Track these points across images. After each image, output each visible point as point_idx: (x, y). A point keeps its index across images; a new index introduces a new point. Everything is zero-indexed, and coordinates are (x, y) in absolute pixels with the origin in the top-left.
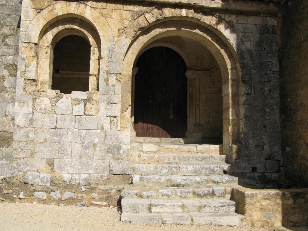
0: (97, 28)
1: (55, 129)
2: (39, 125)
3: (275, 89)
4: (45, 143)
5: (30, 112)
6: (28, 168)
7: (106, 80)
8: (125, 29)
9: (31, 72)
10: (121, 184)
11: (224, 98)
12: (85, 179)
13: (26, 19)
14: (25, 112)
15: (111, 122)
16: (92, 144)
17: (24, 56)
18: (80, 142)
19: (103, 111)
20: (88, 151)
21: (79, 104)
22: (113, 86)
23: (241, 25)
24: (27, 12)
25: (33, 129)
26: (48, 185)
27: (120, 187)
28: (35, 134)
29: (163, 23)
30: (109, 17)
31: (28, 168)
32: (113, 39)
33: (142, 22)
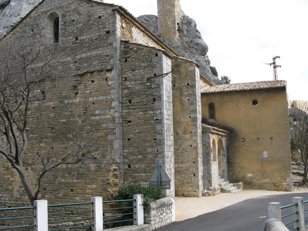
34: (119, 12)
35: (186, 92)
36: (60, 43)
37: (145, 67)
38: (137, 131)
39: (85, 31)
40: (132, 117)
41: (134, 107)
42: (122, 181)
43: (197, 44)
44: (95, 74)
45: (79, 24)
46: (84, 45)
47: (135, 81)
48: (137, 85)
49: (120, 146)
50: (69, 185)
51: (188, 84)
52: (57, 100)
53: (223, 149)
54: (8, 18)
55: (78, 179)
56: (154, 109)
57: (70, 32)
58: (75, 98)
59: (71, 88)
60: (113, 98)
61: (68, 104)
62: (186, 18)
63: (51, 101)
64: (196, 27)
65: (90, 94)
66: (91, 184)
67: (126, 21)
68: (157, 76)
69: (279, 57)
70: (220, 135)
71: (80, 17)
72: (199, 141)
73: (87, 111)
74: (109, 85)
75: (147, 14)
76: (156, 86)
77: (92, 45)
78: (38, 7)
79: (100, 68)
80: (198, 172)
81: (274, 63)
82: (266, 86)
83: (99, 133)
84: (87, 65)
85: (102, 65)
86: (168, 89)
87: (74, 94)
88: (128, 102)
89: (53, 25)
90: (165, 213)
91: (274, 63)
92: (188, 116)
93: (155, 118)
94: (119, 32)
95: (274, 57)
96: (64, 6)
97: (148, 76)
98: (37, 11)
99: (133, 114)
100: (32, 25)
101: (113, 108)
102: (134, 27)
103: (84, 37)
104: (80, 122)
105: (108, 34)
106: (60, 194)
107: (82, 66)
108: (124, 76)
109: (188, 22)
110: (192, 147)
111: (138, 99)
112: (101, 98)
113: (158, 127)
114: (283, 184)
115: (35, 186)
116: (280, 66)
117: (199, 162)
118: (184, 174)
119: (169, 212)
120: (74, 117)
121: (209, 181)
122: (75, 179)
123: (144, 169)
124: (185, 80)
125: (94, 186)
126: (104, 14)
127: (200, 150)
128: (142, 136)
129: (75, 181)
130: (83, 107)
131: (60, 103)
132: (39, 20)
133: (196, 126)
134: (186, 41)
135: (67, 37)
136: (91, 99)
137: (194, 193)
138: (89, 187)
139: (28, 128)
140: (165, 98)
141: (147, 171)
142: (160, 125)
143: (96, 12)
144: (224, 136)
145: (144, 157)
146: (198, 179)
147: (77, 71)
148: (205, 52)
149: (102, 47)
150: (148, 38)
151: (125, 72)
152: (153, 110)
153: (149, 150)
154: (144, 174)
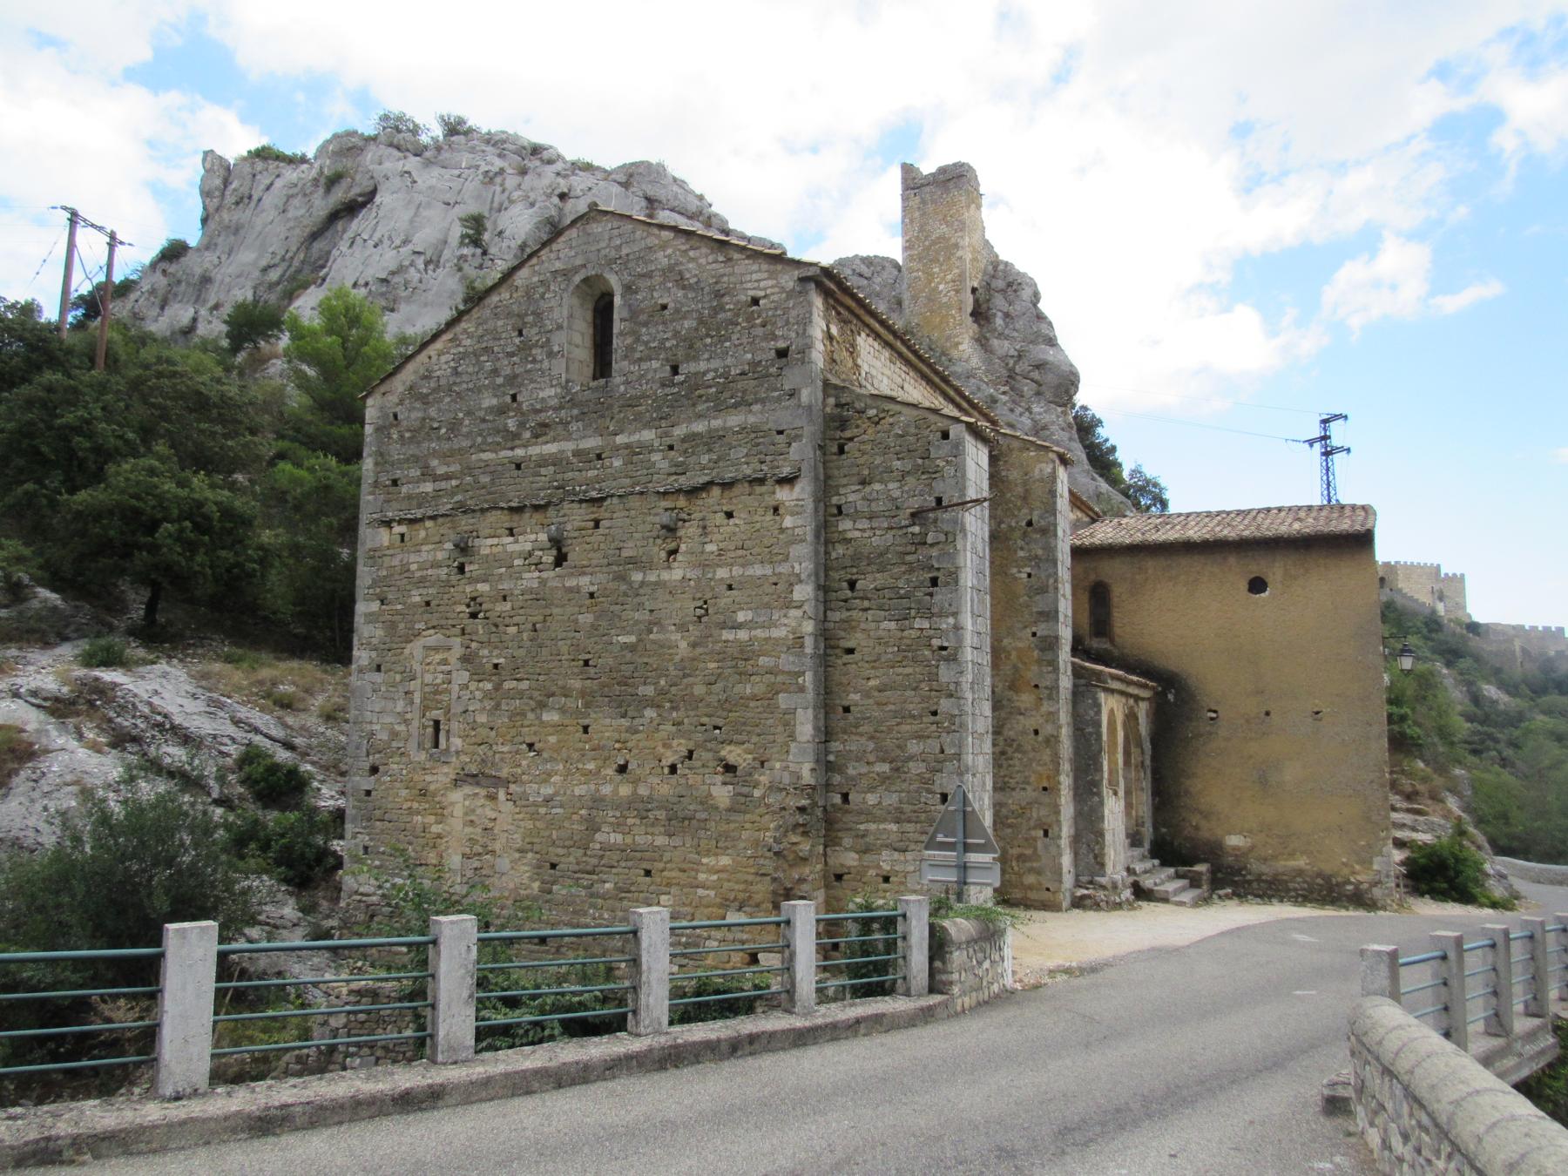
34: (820, 286)
35: (1022, 549)
36: (617, 379)
37: (904, 475)
38: (872, 683)
39: (706, 345)
40: (858, 635)
41: (866, 604)
42: (821, 847)
43: (1040, 366)
44: (737, 490)
45: (684, 318)
46: (701, 392)
47: (870, 518)
48: (878, 532)
49: (816, 728)
50: (638, 855)
51: (1030, 524)
52: (605, 569)
53: (1140, 745)
54: (368, 253)
55: (670, 836)
56: (933, 615)
57: (653, 345)
58: (669, 568)
59: (654, 534)
60: (797, 570)
61: (642, 584)
62: (1004, 271)
63: (584, 574)
64: (1038, 301)
65: (720, 555)
66: (716, 855)
67: (838, 313)
68: (946, 507)
69: (1346, 417)
70: (1131, 696)
71: (685, 296)
72: (1064, 717)
73: (707, 610)
74: (782, 530)
75: (864, 254)
76: (942, 538)
77: (728, 394)
78: (542, 253)
79: (755, 471)
80: (1059, 822)
81: (1325, 438)
82: (1297, 526)
83: (748, 686)
84: (710, 460)
85: (762, 463)
86: (980, 548)
87: (663, 555)
88: (845, 585)
89: (589, 316)
90: (988, 961)
91: (1325, 438)
92: (1029, 631)
93: (936, 642)
94: (818, 356)
95: (1326, 417)
96: (631, 257)
97: (915, 503)
98: (537, 268)
99: (863, 626)
100: (518, 316)
101: (794, 604)
102: (863, 335)
103: (703, 366)
104: (683, 645)
105: (784, 360)
106: (607, 885)
107: (692, 460)
108: (835, 500)
109: (1010, 285)
110: (1040, 738)
111: (881, 579)
112: (758, 570)
113: (945, 674)
114: (1359, 878)
115: (517, 855)
116: (1348, 450)
117: (1062, 787)
118: (1010, 826)
119: (997, 958)
120: (662, 629)
121: (1096, 857)
122: (660, 834)
123: (896, 809)
124: (1020, 510)
125: (725, 861)
126: (768, 292)
127: (1066, 747)
128: (892, 700)
129: (661, 841)
130: (694, 599)
131: (613, 580)
132: (542, 297)
133: (1053, 664)
134: (1000, 352)
135: (640, 359)
136: (722, 573)
137: (1046, 896)
138: (707, 864)
139: (502, 660)
140: (968, 579)
141: (903, 817)
142: (953, 665)
143: (742, 283)
144: (1143, 699)
145: (897, 770)
146: (1059, 846)
147: (675, 477)
148: (1067, 392)
149: (763, 401)
150: (904, 368)
151: (837, 487)
152: (931, 616)
153: (914, 747)
154: (894, 827)
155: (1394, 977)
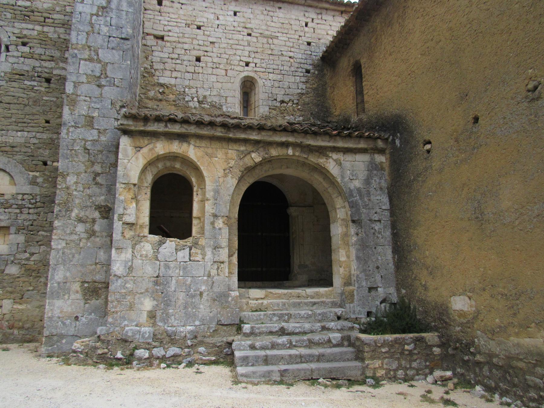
0: (202, 168)
1: (157, 277)
2: (140, 273)
3: (386, 227)
4: (146, 293)
5: (129, 259)
6: (126, 322)
7: (213, 223)
8: (231, 169)
9: (130, 216)
10: (230, 335)
11: (332, 239)
12: (192, 331)
13: (123, 158)
14: (124, 259)
15: (218, 268)
16: (199, 293)
17: (122, 198)
18: (185, 291)
19: (209, 255)
20: (194, 300)
21: (184, 249)
22: (220, 229)
23: (349, 162)
24: (125, 150)
25: (133, 278)
26: (150, 341)
27: (230, 339)
28: (134, 283)
29: (269, 161)
30: (214, 156)
31: (126, 322)
32: (219, 180)
33: (248, 162)
155: (196, 73)
